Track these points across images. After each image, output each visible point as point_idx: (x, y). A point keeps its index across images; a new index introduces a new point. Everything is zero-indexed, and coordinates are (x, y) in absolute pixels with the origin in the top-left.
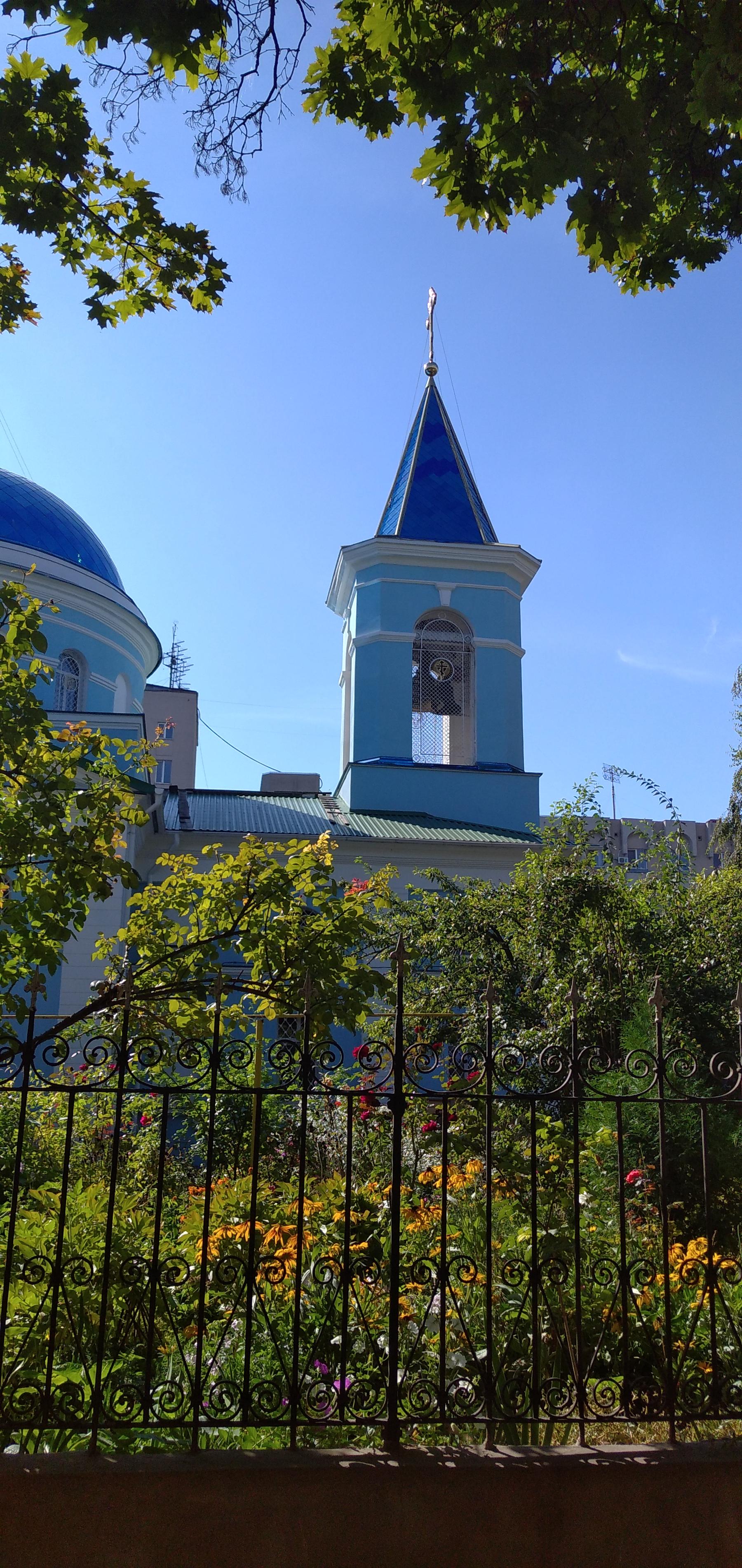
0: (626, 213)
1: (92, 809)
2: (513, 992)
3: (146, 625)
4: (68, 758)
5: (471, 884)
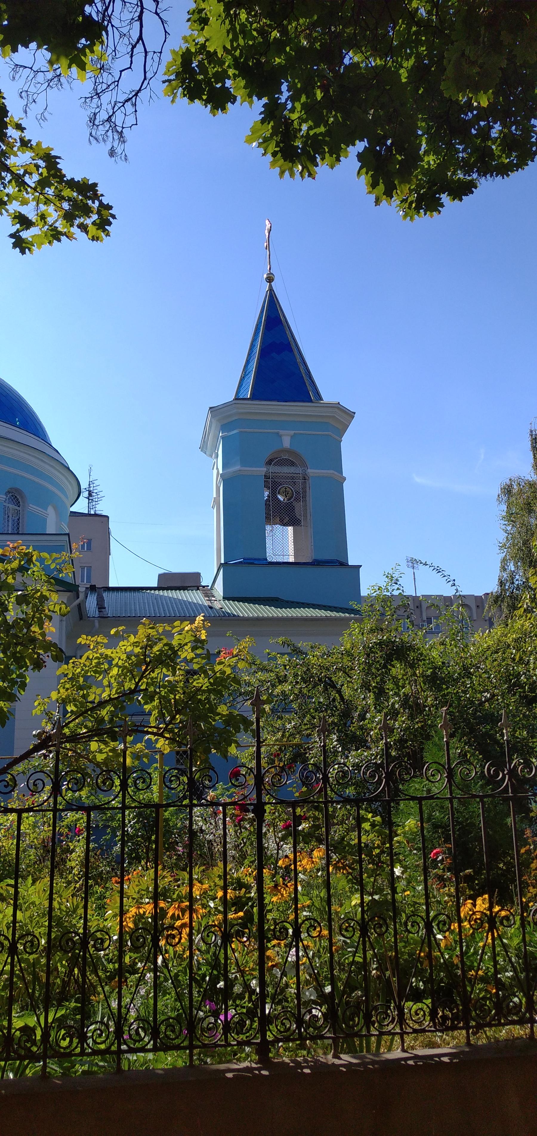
0: (400, 162)
1: (27, 605)
2: (345, 724)
3: (68, 468)
4: (9, 568)
5: (312, 647)
